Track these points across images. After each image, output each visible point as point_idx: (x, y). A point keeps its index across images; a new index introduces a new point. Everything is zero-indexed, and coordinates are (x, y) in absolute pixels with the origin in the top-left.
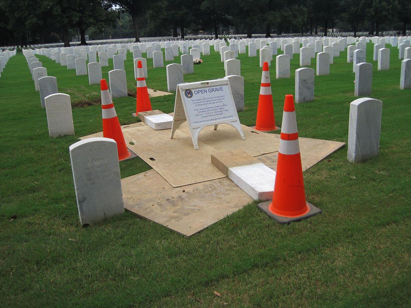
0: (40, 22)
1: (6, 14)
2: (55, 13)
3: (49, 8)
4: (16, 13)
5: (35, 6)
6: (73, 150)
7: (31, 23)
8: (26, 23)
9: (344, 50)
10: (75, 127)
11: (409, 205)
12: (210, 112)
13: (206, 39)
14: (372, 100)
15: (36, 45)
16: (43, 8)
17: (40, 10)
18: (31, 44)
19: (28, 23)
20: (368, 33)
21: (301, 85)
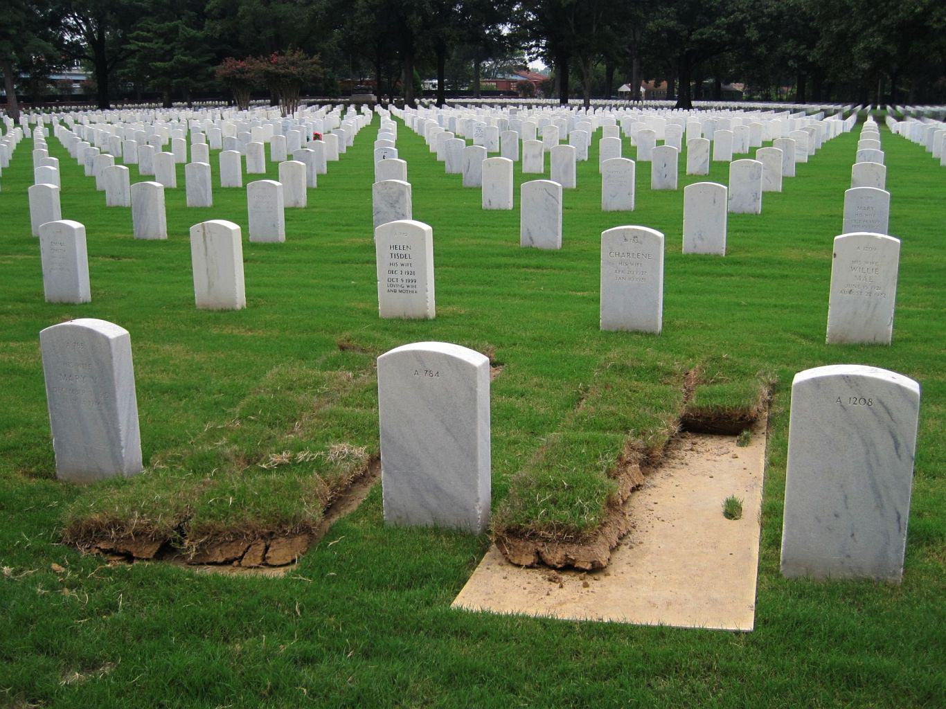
0: (889, 47)
1: (811, 23)
2: (935, 26)
3: (919, 10)
4: (834, 23)
5: (883, 4)
6: (800, 384)
7: (865, 49)
8: (855, 50)
9: (167, 143)
10: (436, 311)
11: (940, 460)
12: (399, 268)
13: (617, 107)
14: (883, 238)
15: (908, 108)
16: (902, 10)
17: (895, 17)
18: (898, 104)
19: (859, 49)
20: (675, 103)
21: (296, 211)
